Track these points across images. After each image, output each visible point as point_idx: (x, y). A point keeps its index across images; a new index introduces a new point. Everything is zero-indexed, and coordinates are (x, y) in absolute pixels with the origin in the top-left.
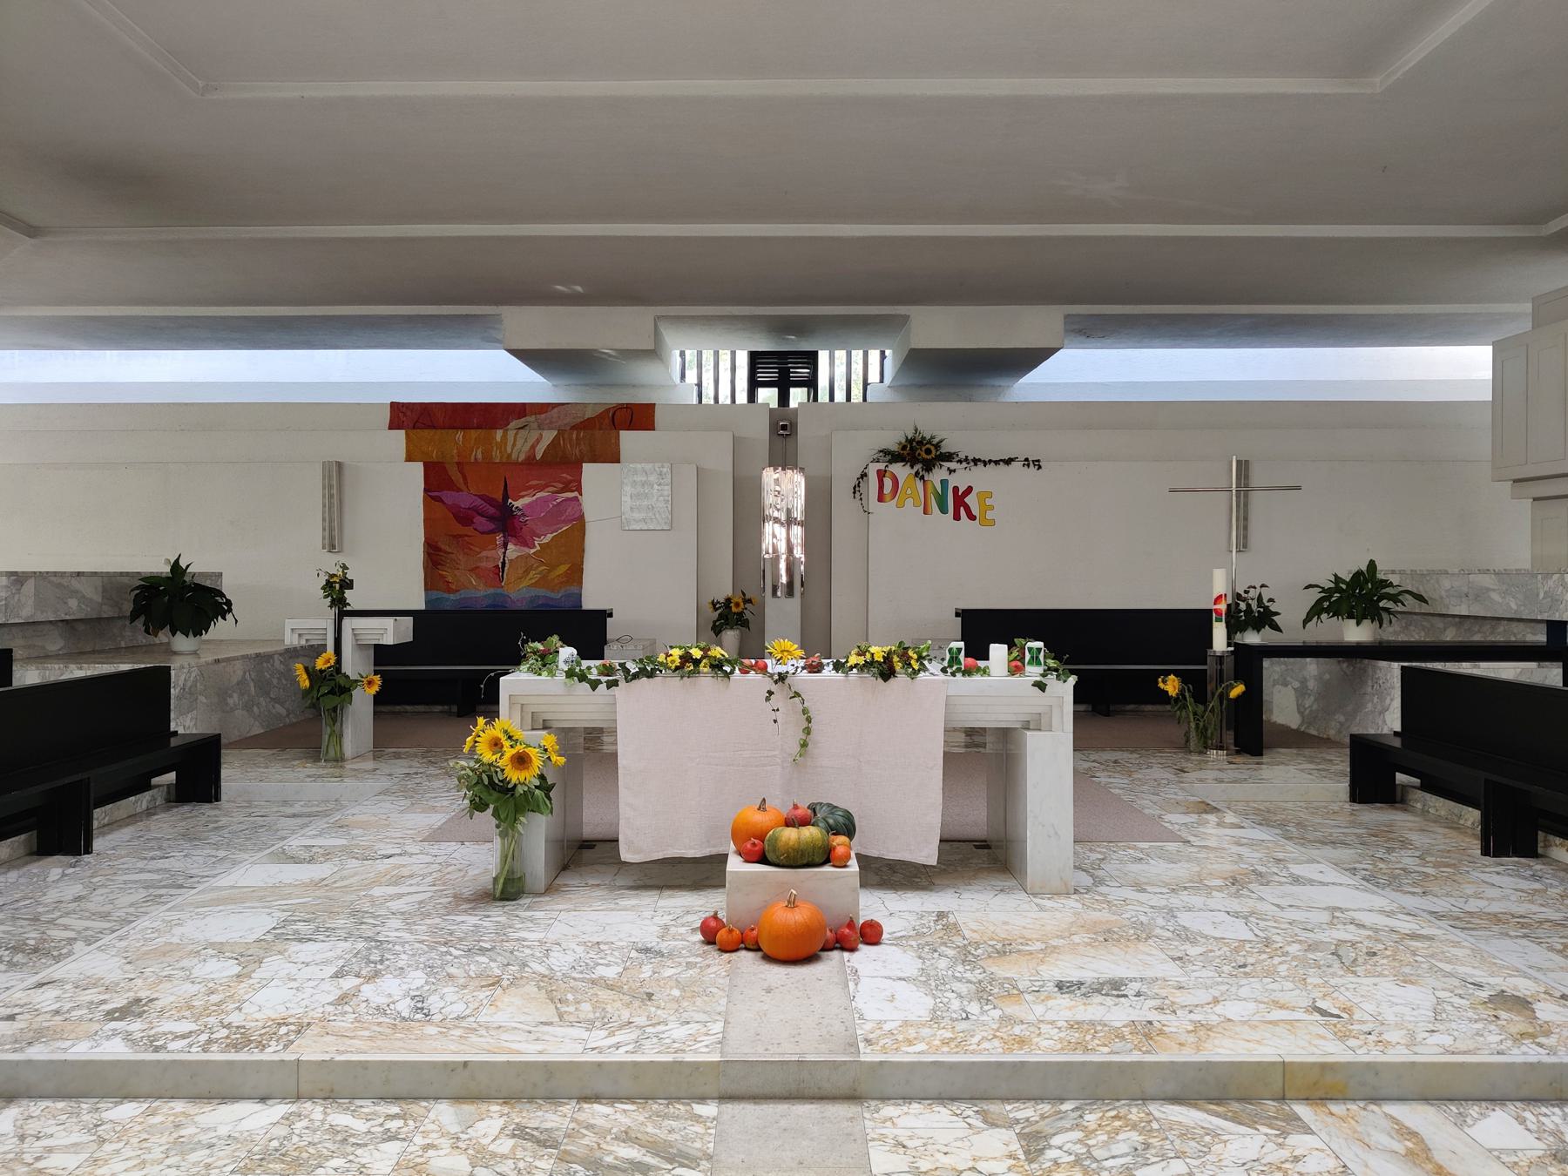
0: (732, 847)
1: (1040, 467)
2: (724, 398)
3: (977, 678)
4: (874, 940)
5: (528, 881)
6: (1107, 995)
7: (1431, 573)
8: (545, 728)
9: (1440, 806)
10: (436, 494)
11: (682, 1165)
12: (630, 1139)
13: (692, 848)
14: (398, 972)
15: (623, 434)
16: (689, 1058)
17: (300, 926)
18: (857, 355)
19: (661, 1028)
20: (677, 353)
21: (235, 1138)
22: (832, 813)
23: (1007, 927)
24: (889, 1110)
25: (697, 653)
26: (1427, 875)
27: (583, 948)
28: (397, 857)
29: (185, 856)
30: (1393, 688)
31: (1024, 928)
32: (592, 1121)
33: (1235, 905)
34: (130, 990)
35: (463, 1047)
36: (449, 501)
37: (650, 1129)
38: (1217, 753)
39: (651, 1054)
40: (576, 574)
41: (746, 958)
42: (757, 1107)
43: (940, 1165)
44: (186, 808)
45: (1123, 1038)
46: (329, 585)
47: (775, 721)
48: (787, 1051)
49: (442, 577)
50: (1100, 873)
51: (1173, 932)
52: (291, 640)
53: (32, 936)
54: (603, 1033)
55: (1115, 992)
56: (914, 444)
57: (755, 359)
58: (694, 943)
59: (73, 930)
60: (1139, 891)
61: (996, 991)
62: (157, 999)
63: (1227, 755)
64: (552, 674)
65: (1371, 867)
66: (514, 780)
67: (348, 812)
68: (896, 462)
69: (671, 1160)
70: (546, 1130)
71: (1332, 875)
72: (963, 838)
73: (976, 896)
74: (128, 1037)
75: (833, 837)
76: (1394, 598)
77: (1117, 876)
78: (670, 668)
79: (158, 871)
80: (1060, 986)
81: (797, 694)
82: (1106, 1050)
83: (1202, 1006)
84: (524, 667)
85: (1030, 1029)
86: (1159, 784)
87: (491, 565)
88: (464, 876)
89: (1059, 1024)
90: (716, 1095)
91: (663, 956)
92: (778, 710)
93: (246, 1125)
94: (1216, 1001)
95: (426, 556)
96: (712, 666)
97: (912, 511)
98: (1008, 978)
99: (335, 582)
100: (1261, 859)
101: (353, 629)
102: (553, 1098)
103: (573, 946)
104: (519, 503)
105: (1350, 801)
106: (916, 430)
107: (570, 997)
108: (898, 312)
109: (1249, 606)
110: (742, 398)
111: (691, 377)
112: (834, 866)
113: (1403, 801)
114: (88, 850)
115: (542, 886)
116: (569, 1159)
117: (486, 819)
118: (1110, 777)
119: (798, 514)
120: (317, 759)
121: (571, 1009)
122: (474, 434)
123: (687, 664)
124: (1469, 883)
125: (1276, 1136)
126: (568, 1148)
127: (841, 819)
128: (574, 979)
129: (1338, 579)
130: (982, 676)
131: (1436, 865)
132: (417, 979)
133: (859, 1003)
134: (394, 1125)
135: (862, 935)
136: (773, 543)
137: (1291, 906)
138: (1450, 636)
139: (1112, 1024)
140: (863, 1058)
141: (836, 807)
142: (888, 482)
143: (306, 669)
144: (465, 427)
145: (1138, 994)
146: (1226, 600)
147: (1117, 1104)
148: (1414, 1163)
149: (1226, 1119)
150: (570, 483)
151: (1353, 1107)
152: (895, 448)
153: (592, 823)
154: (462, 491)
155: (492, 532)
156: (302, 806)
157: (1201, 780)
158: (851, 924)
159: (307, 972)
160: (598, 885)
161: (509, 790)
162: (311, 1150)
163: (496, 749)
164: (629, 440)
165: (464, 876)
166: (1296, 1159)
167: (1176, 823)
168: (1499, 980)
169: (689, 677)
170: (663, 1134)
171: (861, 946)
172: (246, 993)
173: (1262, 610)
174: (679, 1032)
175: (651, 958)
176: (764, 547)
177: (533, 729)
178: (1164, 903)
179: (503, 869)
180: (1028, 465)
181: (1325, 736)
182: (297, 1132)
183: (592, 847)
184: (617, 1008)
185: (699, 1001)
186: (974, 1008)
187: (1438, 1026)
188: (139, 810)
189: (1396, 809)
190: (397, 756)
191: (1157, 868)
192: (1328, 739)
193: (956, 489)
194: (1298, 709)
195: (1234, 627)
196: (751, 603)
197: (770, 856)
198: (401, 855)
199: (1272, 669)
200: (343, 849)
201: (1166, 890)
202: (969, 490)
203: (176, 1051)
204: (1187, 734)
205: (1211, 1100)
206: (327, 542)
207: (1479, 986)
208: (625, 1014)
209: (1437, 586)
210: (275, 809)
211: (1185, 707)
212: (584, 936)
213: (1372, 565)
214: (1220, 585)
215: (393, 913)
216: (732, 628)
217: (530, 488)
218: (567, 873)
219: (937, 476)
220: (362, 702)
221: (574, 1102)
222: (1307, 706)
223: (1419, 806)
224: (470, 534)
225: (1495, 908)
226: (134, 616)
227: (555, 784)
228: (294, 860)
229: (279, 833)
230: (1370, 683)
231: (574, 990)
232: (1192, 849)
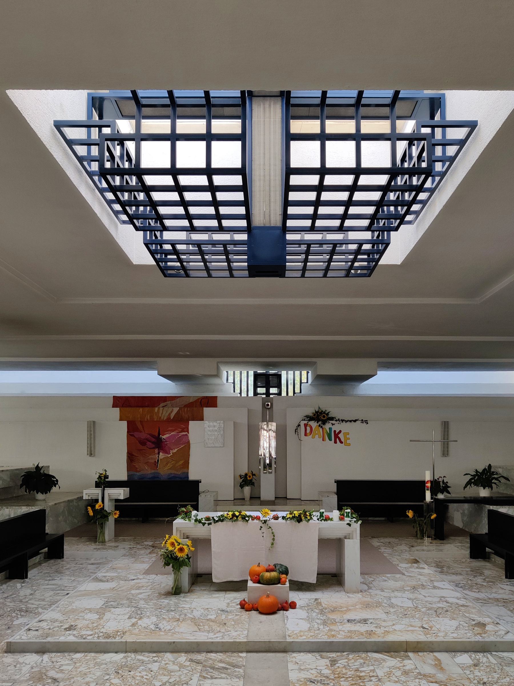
0: (249, 578)
1: (367, 423)
3: (329, 522)
4: (294, 607)
5: (183, 588)
6: (362, 623)
8: (187, 538)
11: (236, 668)
12: (222, 662)
14: (147, 617)
16: (238, 640)
17: (112, 603)
18: (297, 373)
19: (229, 633)
21: (112, 662)
22: (281, 567)
23: (336, 603)
24: (294, 655)
25: (237, 514)
27: (203, 610)
28: (136, 580)
29: (60, 579)
31: (342, 603)
32: (211, 658)
33: (411, 596)
34: (68, 623)
35: (172, 638)
37: (227, 659)
38: (427, 539)
39: (226, 639)
40: (186, 464)
41: (254, 613)
42: (257, 654)
43: (306, 667)
44: (52, 561)
45: (363, 635)
47: (263, 537)
48: (266, 639)
50: (371, 585)
51: (388, 605)
53: (23, 607)
54: (213, 634)
55: (364, 623)
56: (319, 413)
57: (256, 376)
58: (238, 608)
59: (35, 605)
60: (382, 591)
61: (329, 622)
62: (77, 625)
63: (431, 540)
65: (466, 582)
67: (114, 563)
68: (311, 421)
69: (233, 667)
70: (198, 660)
71: (447, 585)
74: (74, 635)
75: (281, 575)
76: (496, 479)
78: (228, 519)
79: (53, 585)
80: (348, 621)
81: (270, 527)
82: (357, 638)
83: (389, 626)
85: (337, 633)
86: (402, 552)
87: (153, 461)
88: (160, 587)
89: (345, 631)
90: (246, 651)
91: (228, 612)
93: (113, 659)
94: (394, 625)
95: (128, 457)
96: (242, 518)
97: (318, 440)
98: (333, 619)
99: (102, 477)
100: (426, 580)
102: (199, 652)
103: (200, 609)
104: (164, 437)
106: (319, 408)
107: (201, 624)
108: (312, 361)
110: (251, 394)
111: (231, 380)
112: (281, 584)
113: (489, 558)
114: (27, 578)
115: (187, 590)
116: (206, 666)
117: (170, 568)
118: (385, 549)
120: (95, 542)
121: (202, 627)
122: (147, 409)
124: (495, 588)
125: (401, 660)
126: (205, 664)
127: (284, 569)
128: (202, 619)
132: (154, 619)
133: (287, 626)
134: (156, 659)
135: (290, 605)
137: (429, 596)
139: (361, 631)
140: (287, 640)
142: (308, 429)
145: (371, 623)
147: (359, 653)
148: (436, 667)
149: (388, 657)
150: (184, 429)
151: (425, 653)
152: (311, 415)
153: (201, 567)
154: (142, 432)
155: (154, 448)
157: (417, 550)
158: (286, 602)
159: (120, 617)
160: (205, 590)
162: (134, 665)
164: (207, 411)
165: (160, 587)
166: (404, 666)
167: (403, 567)
168: (481, 619)
170: (231, 661)
172: (104, 623)
174: (235, 634)
177: (184, 538)
178: (389, 595)
180: (363, 422)
182: (129, 660)
183: (201, 576)
184: (215, 627)
185: (240, 625)
186: (321, 627)
187: (456, 632)
188: (36, 562)
189: (486, 561)
190: (124, 541)
191: (391, 584)
193: (335, 431)
194: (462, 521)
197: (261, 581)
198: (137, 579)
199: (452, 507)
200: (117, 577)
202: (340, 432)
203: (90, 639)
204: (417, 532)
205: (386, 652)
206: (89, 452)
208: (218, 629)
210: (85, 561)
213: (490, 466)
214: (428, 477)
215: (140, 599)
216: (247, 486)
218: (194, 585)
219: (327, 426)
221: (205, 653)
222: (465, 520)
223: (493, 560)
225: (499, 596)
226: (21, 486)
228: (101, 581)
229: (90, 571)
230: (484, 513)
231: (202, 622)
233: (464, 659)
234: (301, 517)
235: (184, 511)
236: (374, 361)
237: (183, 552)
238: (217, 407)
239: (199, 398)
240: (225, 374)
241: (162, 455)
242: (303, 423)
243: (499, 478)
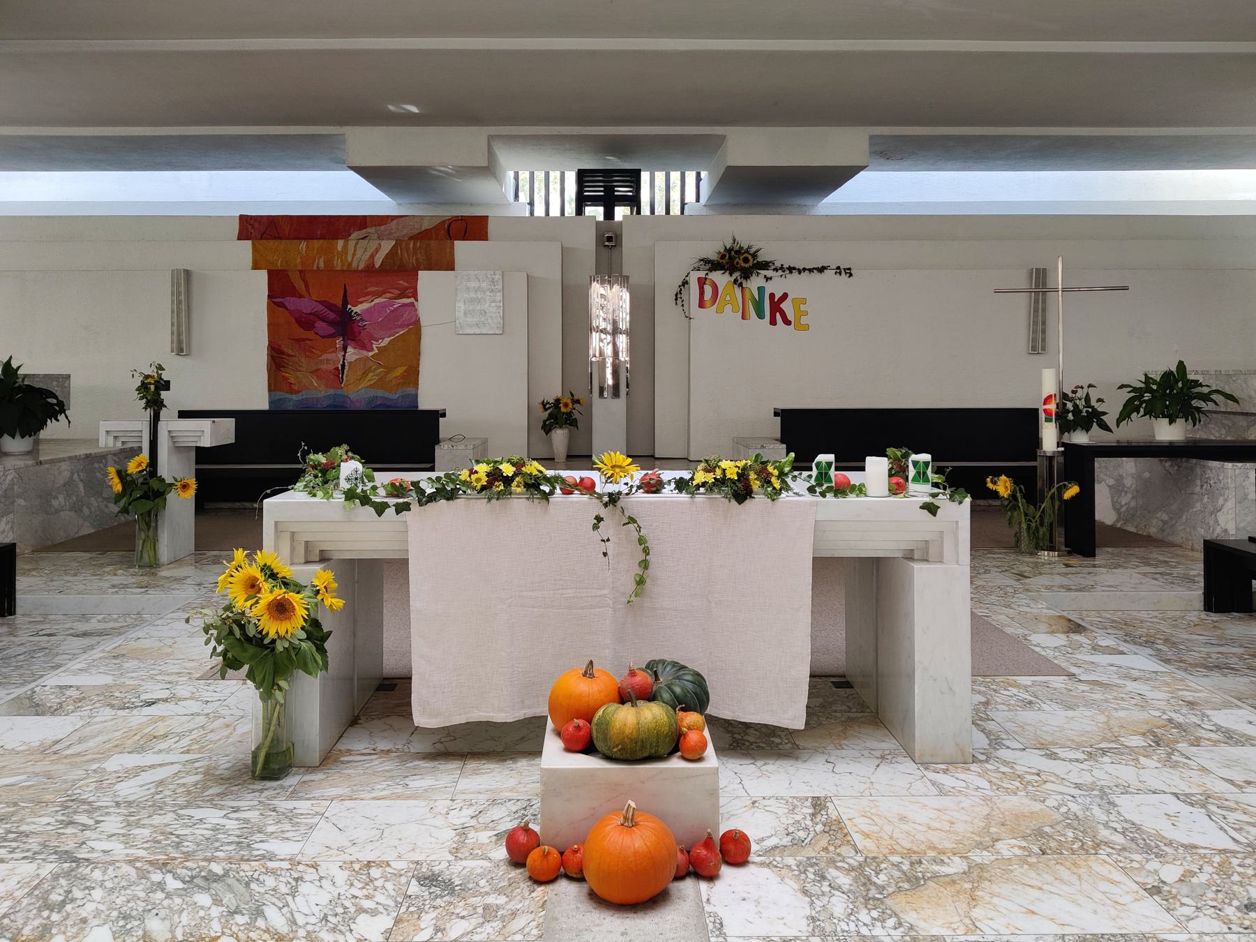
2: (555, 211)
3: (852, 498)
4: (739, 860)
5: (299, 751)
7: (1238, 373)
10: (280, 300)
13: (502, 711)
15: (456, 243)
18: (675, 176)
20: (511, 174)
22: (678, 678)
25: (508, 470)
30: (1227, 488)
33: (1176, 780)
36: (292, 307)
38: (1048, 555)
40: (412, 375)
46: (144, 387)
47: (605, 554)
49: (286, 379)
52: (106, 443)
63: (1059, 556)
64: (328, 495)
66: (272, 635)
67: (131, 636)
68: (715, 270)
72: (824, 674)
73: (854, 767)
75: (681, 714)
76: (1206, 398)
77: (1014, 732)
78: (474, 488)
81: (632, 520)
84: (300, 485)
87: (331, 367)
92: (608, 540)
96: (527, 486)
97: (731, 316)
99: (150, 384)
101: (169, 431)
104: (358, 309)
105: (1205, 610)
108: (715, 133)
109: (1076, 406)
110: (570, 209)
111: (524, 197)
115: (316, 757)
119: (624, 325)
122: (316, 244)
123: (496, 483)
127: (690, 686)
130: (857, 496)
136: (600, 347)
141: (683, 667)
142: (708, 290)
143: (119, 473)
144: (309, 237)
146: (1055, 400)
155: (332, 336)
156: (99, 621)
157: (1048, 588)
158: (708, 842)
161: (266, 647)
163: (251, 592)
164: (463, 249)
169: (498, 499)
171: (725, 870)
173: (1090, 410)
175: (436, 897)
176: (591, 352)
177: (307, 562)
179: (265, 737)
180: (840, 273)
181: (1145, 534)
193: (772, 296)
194: (1113, 505)
195: (1065, 426)
196: (579, 403)
197: (599, 745)
198: (165, 700)
201: (1082, 756)
202: (785, 296)
209: (1244, 385)
211: (1016, 508)
212: (352, 850)
213: (1181, 365)
219: (755, 283)
220: (180, 505)
222: (1123, 503)
224: (311, 338)
227: (331, 632)
230: (1198, 482)
232: (1082, 687)
234: (748, 480)
235: (320, 464)
237: (289, 618)
239: (443, 219)
241: (354, 354)
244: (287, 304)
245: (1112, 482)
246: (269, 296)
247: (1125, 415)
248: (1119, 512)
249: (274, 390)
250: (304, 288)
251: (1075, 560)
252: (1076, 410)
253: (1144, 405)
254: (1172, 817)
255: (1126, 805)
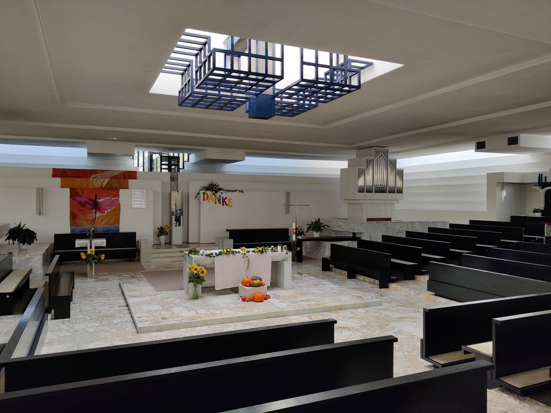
3: (276, 252)
9: (338, 270)
25: (229, 250)
26: (340, 283)
33: (317, 289)
40: (117, 221)
56: (212, 186)
68: (208, 190)
76: (323, 227)
87: (91, 219)
97: (212, 203)
106: (212, 182)
109: (299, 230)
122: (83, 179)
129: (312, 222)
131: (341, 281)
138: (334, 235)
142: (206, 196)
152: (206, 186)
164: (131, 182)
192: (312, 258)
193: (223, 198)
195: (297, 235)
197: (252, 286)
202: (226, 198)
207: (355, 295)
217: (103, 196)
219: (218, 194)
224: (84, 209)
225: (352, 287)
233: (360, 310)
236: (243, 151)
238: (136, 179)
239: (122, 172)
240: (136, 155)
242: (202, 192)
243: (324, 226)
244: (76, 199)
245: (305, 246)
246: (70, 197)
247: (307, 231)
248: (306, 253)
249: (72, 226)
250: (82, 194)
251: (299, 263)
252: (299, 231)
253: (311, 228)
254: (316, 291)
255: (311, 291)
